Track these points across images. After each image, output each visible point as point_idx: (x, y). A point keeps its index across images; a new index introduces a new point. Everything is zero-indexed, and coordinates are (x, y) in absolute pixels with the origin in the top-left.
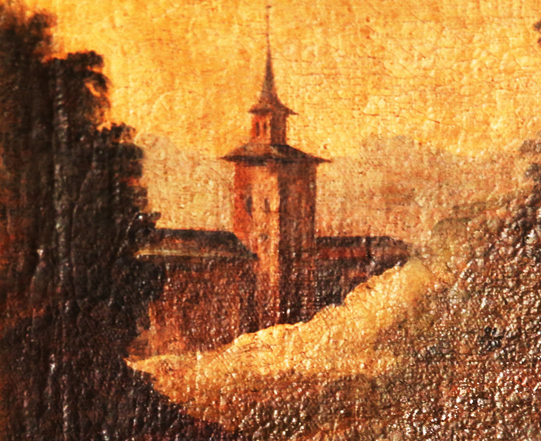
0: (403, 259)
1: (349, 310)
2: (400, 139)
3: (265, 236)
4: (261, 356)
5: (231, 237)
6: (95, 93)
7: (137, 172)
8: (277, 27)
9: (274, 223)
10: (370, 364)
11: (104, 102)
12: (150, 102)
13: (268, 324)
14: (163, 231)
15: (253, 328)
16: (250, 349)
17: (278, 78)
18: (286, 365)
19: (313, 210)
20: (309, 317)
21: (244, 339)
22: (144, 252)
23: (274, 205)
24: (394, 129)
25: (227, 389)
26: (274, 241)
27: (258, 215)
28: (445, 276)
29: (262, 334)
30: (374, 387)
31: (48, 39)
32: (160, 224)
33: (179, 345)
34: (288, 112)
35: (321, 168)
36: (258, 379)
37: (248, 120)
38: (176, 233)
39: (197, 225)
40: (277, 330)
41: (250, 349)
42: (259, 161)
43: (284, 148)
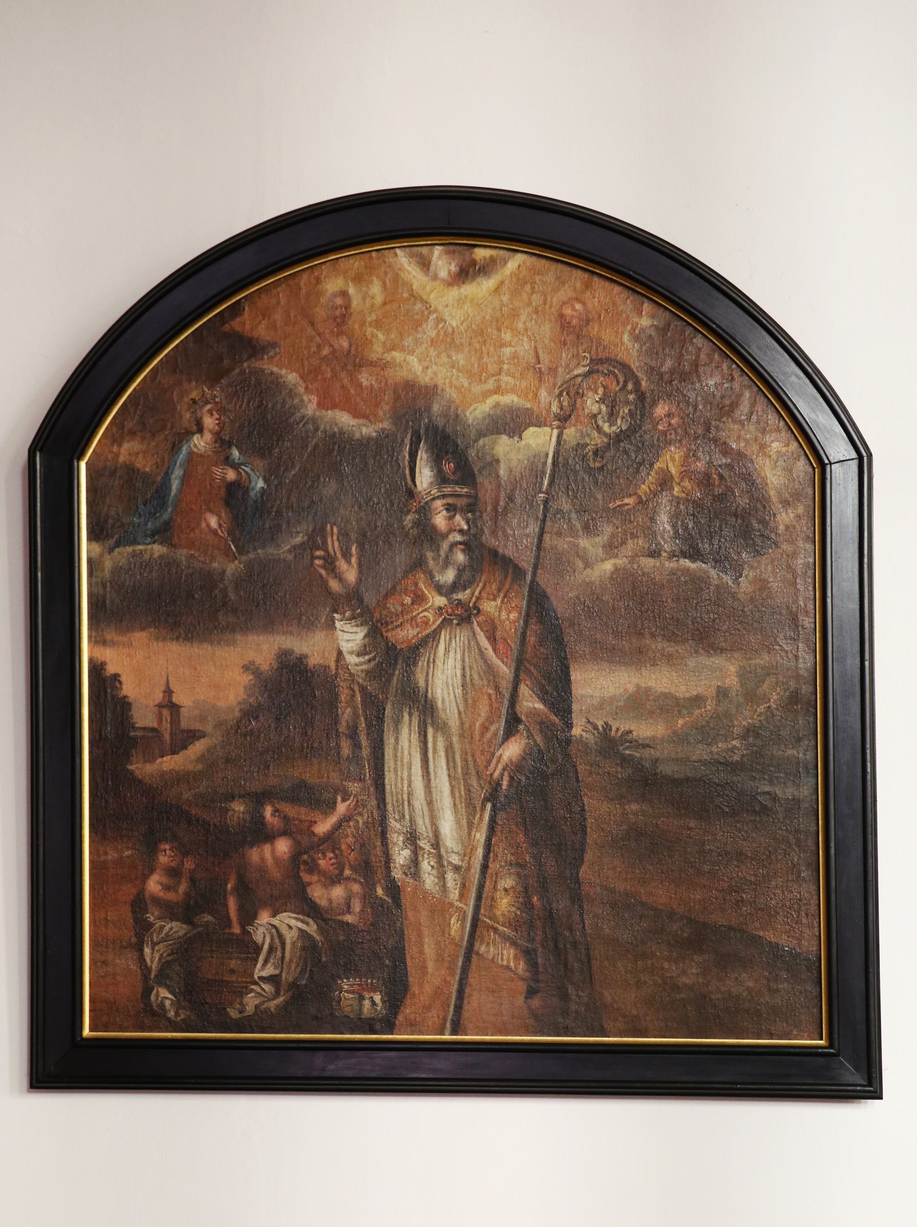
0: (204, 737)
1: (435, 373)
2: (204, 701)
3: (166, 729)
4: (165, 765)
5: (156, 729)
6: (118, 686)
7: (130, 710)
8: (170, 668)
9: (169, 725)
10: (195, 767)
11: (121, 689)
12: (134, 689)
13: (752, 542)
14: (137, 728)
15: (163, 757)
16: (161, 763)
17: (170, 682)
18: (172, 767)
19: (179, 721)
20: (178, 753)
21: (160, 760)
22: (132, 734)
23: (169, 720)
24: (202, 698)
25: (155, 775)
26: (169, 731)
27: (164, 723)
28: (665, 646)
29: (165, 759)
30: (195, 774)
31: (105, 669)
32: (137, 725)
33: (142, 762)
34: (173, 692)
35: (182, 709)
36: (164, 771)
37: (161, 695)
38: (141, 728)
39: (147, 726)
40: (169, 757)
41: (161, 763)
42: (165, 707)
43: (171, 702)
